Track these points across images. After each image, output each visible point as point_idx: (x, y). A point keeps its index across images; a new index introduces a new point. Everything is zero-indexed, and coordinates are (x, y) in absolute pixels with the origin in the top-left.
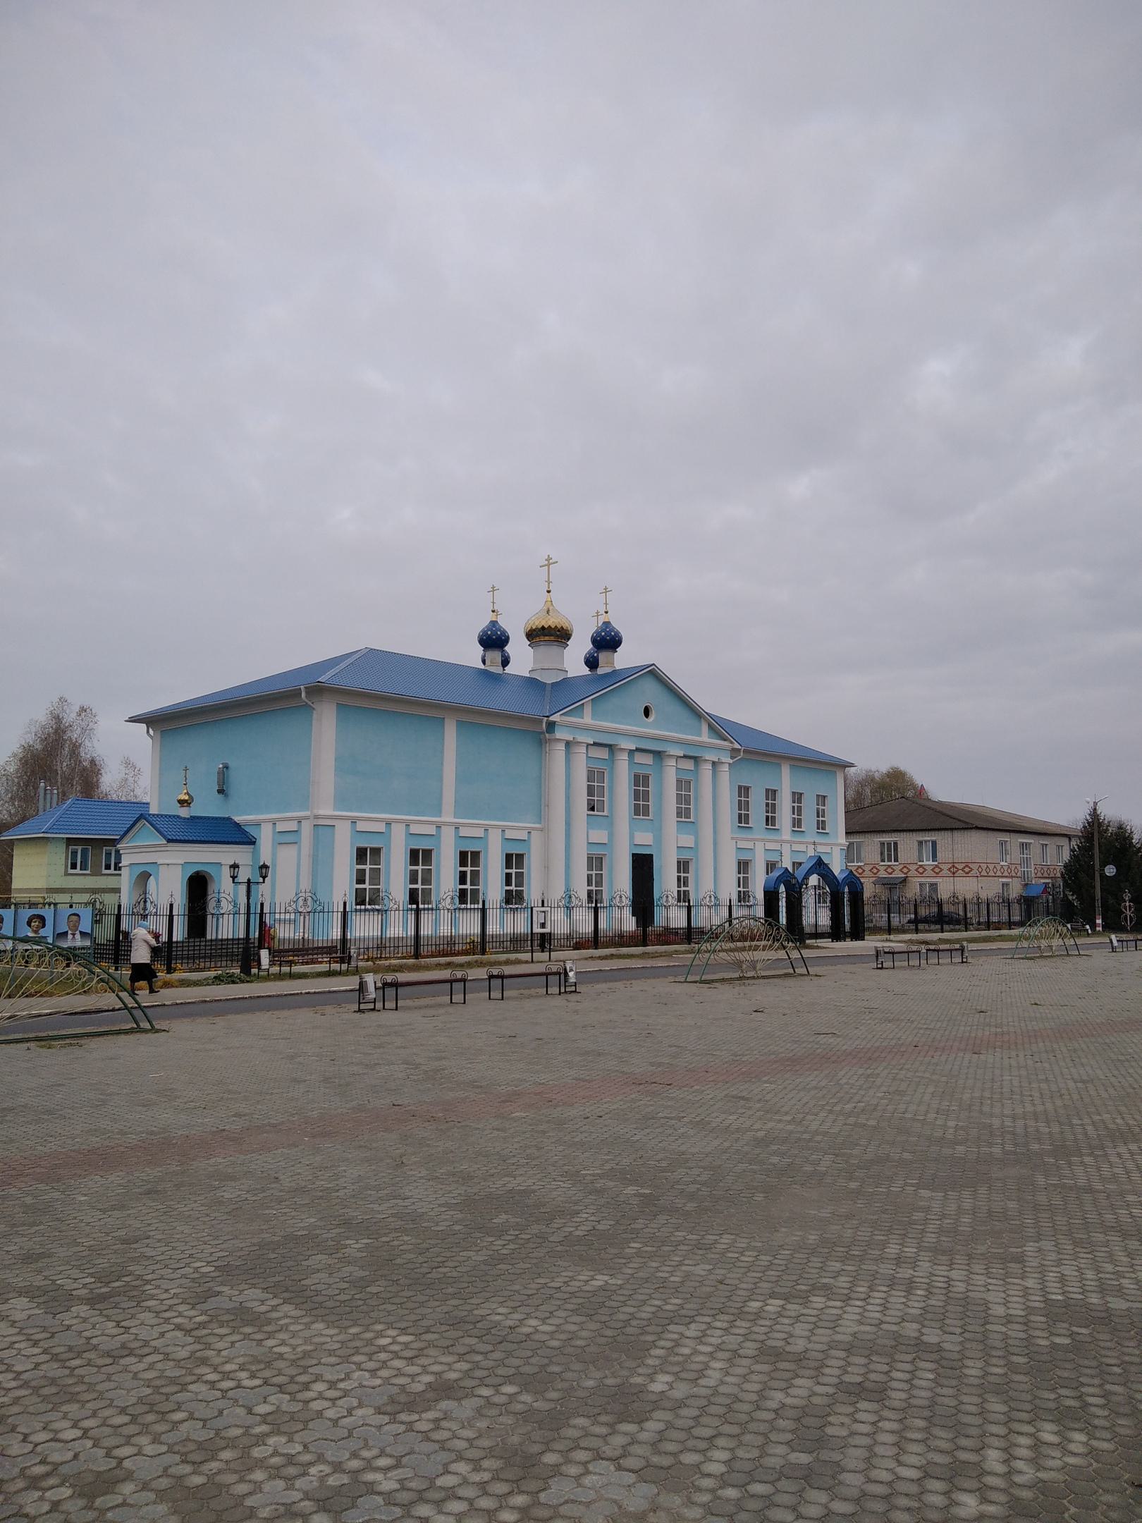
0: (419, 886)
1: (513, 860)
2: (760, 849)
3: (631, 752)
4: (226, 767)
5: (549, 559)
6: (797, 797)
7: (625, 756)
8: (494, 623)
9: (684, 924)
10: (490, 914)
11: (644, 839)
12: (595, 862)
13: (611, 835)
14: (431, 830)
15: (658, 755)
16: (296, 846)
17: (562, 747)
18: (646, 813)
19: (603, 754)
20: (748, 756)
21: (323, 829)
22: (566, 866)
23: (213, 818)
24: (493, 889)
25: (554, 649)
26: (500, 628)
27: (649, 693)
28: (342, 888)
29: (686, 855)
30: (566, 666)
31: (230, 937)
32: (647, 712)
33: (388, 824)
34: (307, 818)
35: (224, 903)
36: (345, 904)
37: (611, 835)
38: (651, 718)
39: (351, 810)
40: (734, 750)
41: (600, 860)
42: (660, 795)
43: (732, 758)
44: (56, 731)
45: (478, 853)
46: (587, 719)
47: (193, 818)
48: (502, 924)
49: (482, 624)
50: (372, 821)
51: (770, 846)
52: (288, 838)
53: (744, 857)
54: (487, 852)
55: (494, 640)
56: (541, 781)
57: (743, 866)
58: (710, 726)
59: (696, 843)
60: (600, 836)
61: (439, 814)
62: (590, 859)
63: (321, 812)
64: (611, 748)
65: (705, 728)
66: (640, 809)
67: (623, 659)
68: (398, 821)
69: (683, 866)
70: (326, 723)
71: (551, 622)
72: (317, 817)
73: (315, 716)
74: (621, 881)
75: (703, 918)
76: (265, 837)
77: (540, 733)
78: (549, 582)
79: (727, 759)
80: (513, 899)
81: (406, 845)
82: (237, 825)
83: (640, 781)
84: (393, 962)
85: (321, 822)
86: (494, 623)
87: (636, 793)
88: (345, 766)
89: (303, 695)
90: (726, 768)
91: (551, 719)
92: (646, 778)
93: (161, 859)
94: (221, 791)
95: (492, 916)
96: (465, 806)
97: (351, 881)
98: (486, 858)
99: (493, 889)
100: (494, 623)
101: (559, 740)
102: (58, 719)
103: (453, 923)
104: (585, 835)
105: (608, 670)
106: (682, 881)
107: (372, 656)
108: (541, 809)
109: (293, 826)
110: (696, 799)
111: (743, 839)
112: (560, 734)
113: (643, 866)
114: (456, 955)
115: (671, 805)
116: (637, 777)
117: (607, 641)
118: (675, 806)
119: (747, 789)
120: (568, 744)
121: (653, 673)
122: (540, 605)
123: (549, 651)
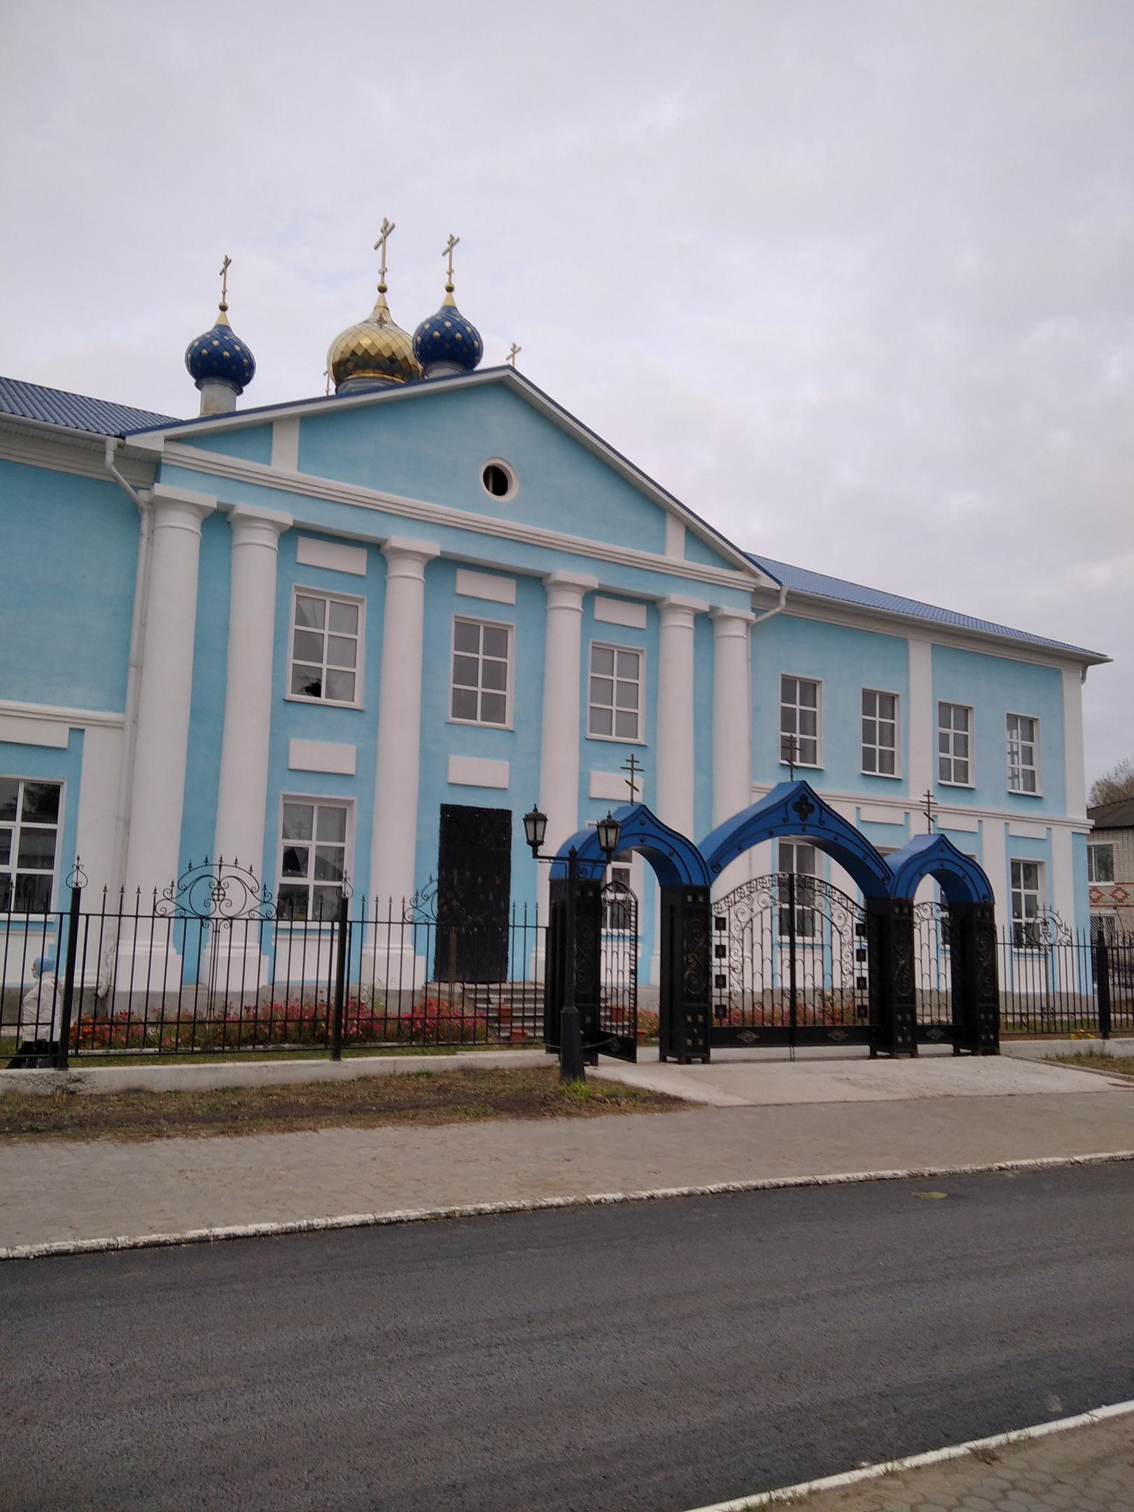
3: (591, 595)
6: (953, 715)
7: (573, 600)
8: (223, 330)
11: (480, 774)
15: (535, 584)
18: (495, 709)
35: (234, 892)
42: (539, 676)
49: (204, 325)
56: (127, 610)
65: (675, 535)
74: (396, 869)
79: (738, 608)
81: (424, 792)
90: (738, 629)
98: (76, 798)
108: (121, 677)
110: (278, 643)
111: (947, 811)
116: (466, 633)
118: (509, 693)
122: (364, 310)
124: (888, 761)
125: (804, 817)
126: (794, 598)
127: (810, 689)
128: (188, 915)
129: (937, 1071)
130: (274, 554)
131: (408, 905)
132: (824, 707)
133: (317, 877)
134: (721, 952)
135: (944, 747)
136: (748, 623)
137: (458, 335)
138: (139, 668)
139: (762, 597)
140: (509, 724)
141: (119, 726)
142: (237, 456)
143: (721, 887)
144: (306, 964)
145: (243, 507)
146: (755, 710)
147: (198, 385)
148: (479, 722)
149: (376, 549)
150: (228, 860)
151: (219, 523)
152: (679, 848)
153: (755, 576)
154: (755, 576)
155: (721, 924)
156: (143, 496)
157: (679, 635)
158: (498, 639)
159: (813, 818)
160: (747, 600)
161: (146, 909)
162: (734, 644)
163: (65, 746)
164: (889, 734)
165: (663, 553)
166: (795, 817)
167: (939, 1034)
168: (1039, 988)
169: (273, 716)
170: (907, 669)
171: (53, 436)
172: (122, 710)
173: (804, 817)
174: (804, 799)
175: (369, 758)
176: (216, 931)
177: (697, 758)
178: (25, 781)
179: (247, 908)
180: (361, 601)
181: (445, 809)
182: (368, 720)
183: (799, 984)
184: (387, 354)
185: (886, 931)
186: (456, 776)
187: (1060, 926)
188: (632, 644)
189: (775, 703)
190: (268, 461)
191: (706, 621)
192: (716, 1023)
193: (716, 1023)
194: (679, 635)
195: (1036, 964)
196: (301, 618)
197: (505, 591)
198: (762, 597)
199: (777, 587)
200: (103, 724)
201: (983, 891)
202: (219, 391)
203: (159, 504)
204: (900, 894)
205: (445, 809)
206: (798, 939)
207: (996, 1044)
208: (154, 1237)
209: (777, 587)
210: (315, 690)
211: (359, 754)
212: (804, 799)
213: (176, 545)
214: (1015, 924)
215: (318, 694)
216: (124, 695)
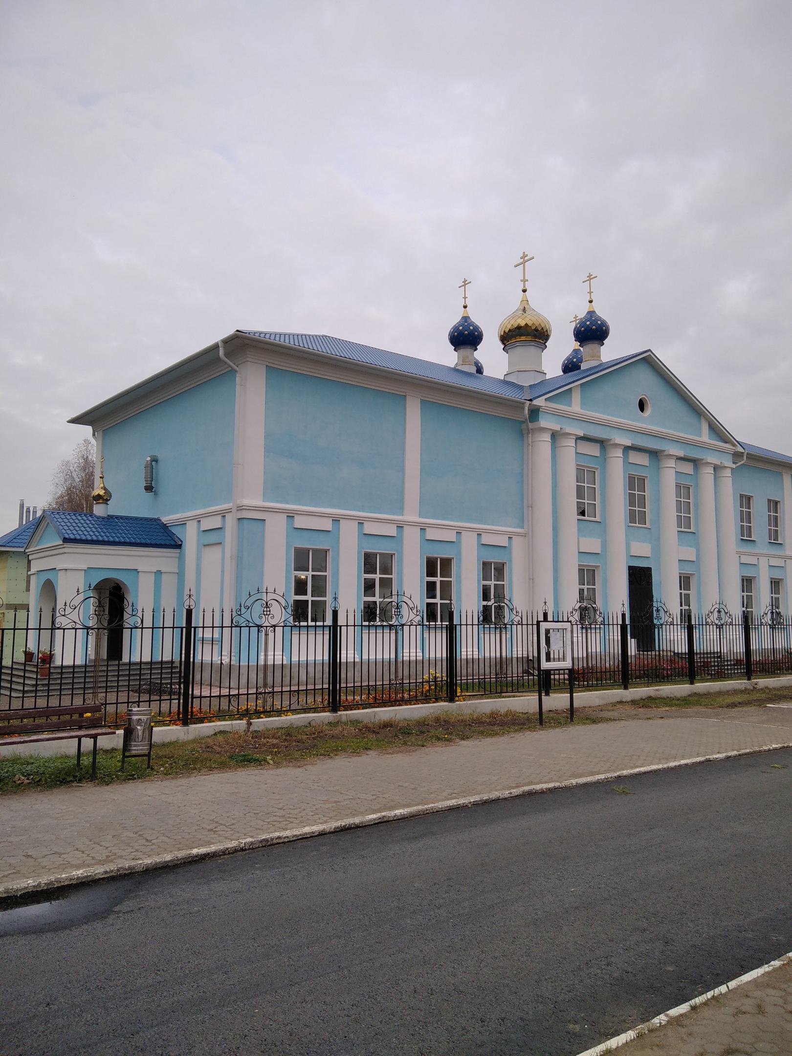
1: (493, 569)
2: (763, 564)
3: (627, 449)
4: (155, 460)
5: (524, 256)
7: (619, 453)
9: (683, 648)
11: (642, 550)
12: (587, 575)
13: (604, 545)
15: (655, 454)
16: (178, 551)
17: (547, 437)
18: (643, 519)
19: (594, 450)
20: (752, 463)
21: (251, 523)
22: (553, 576)
23: (146, 519)
24: (468, 602)
25: (531, 350)
26: (472, 324)
27: (644, 383)
29: (688, 570)
30: (545, 369)
31: (147, 658)
32: (642, 406)
33: (336, 521)
34: (229, 511)
35: (275, 609)
37: (604, 545)
38: (648, 412)
39: (287, 503)
41: (592, 572)
42: (658, 500)
44: (84, 469)
46: (576, 406)
48: (477, 646)
49: (453, 320)
50: (315, 516)
51: (775, 562)
52: (212, 538)
53: (749, 573)
54: (460, 560)
55: (465, 338)
57: (747, 583)
59: (698, 556)
60: (592, 545)
61: (401, 510)
62: (581, 571)
63: (247, 502)
64: (602, 443)
66: (636, 517)
67: (610, 351)
69: (685, 582)
70: (252, 387)
72: (240, 508)
74: (616, 600)
75: (708, 641)
76: (190, 537)
78: (524, 281)
79: (728, 462)
80: (492, 617)
82: (165, 527)
83: (635, 483)
85: (246, 514)
86: (466, 319)
87: (632, 497)
88: (275, 446)
90: (728, 473)
91: (535, 402)
92: (642, 480)
93: (59, 562)
94: (149, 488)
95: (348, 637)
96: (427, 505)
98: (459, 567)
99: (468, 602)
100: (466, 319)
102: (86, 460)
103: (286, 646)
104: (576, 542)
105: (594, 363)
106: (685, 600)
108: (523, 511)
109: (216, 522)
111: (745, 554)
112: (544, 422)
113: (640, 580)
114: (402, 702)
115: (670, 514)
117: (592, 332)
119: (749, 498)
120: (555, 436)
121: (647, 361)
122: (514, 305)
123: (524, 352)
126: (751, 457)
128: (251, 625)
131: (234, 614)
133: (441, 599)
139: (737, 456)
141: (524, 535)
147: (455, 350)
148: (637, 525)
150: (271, 590)
153: (734, 445)
168: (388, 655)
170: (783, 489)
171: (306, 356)
172: (522, 527)
176: (267, 635)
178: (495, 563)
179: (283, 620)
180: (597, 469)
183: (753, 646)
184: (533, 328)
186: (634, 553)
187: (726, 613)
188: (688, 483)
195: (493, 636)
198: (737, 456)
200: (518, 534)
202: (466, 351)
208: (452, 802)
209: (743, 451)
214: (428, 604)
215: (584, 515)
216: (523, 521)
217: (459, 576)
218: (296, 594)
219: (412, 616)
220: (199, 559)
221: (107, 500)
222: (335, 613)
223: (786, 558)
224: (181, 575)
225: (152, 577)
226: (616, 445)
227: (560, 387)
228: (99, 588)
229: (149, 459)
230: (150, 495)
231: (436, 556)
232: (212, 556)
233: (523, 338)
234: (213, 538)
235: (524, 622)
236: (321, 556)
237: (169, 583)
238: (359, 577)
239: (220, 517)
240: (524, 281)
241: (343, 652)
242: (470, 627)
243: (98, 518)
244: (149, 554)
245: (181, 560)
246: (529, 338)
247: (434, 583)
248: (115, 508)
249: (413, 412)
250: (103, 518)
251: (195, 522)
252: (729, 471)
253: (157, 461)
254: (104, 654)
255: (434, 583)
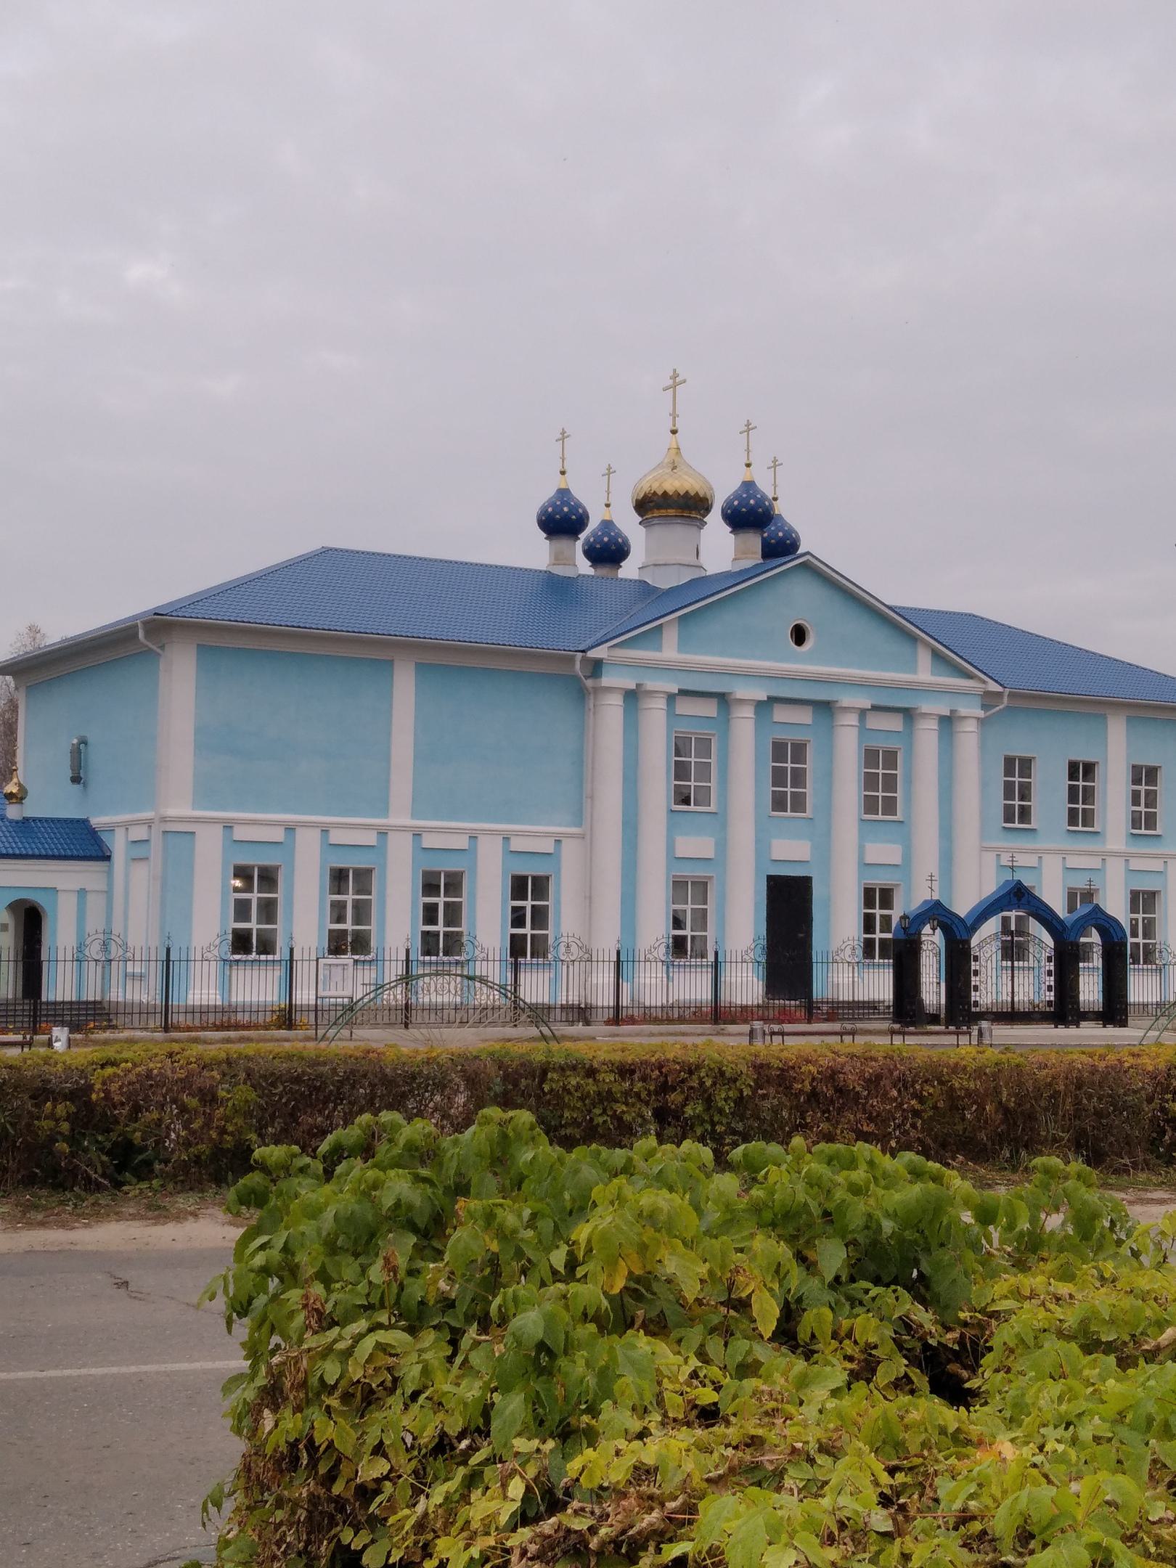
0: (527, 930)
1: (528, 889)
3: (671, 698)
7: (852, 719)
8: (564, 493)
10: (298, 967)
11: (792, 852)
14: (370, 838)
15: (825, 708)
16: (106, 863)
17: (616, 701)
21: (179, 838)
28: (209, 922)
32: (799, 635)
35: (574, 948)
36: (408, 951)
39: (224, 809)
40: (988, 694)
42: (828, 776)
43: (985, 707)
45: (369, 872)
46: (669, 650)
47: (26, 820)
49: (542, 495)
50: (260, 826)
58: (936, 655)
60: (696, 845)
61: (385, 811)
63: (172, 812)
65: (924, 658)
68: (306, 825)
70: (180, 677)
71: (672, 484)
72: (164, 820)
73: (161, 667)
74: (741, 926)
76: (118, 846)
77: (576, 680)
78: (674, 416)
84: (138, 1034)
88: (210, 741)
89: (141, 634)
90: (971, 726)
94: (76, 779)
95: (304, 973)
97: (414, 918)
98: (558, 884)
101: (609, 689)
103: (226, 985)
107: (329, 565)
108: (580, 807)
110: (909, 781)
113: (789, 902)
116: (779, 750)
118: (809, 790)
123: (674, 535)
124: (1088, 818)
125: (1019, 900)
127: (1026, 765)
129: (1091, 1034)
130: (621, 710)
132: (1037, 779)
134: (976, 973)
135: (1136, 801)
136: (978, 719)
137: (752, 502)
138: (592, 798)
140: (809, 814)
141: (583, 837)
142: (646, 649)
143: (974, 941)
144: (693, 987)
145: (650, 685)
146: (984, 785)
149: (723, 699)
151: (633, 697)
152: (956, 921)
153: (984, 682)
154: (984, 682)
155: (976, 959)
156: (589, 683)
157: (927, 734)
158: (799, 751)
159: (1024, 900)
160: (978, 701)
161: (642, 959)
162: (969, 736)
163: (551, 851)
164: (1089, 795)
165: (915, 672)
166: (1014, 900)
167: (1091, 1016)
169: (860, 830)
172: (580, 825)
173: (1019, 900)
174: (1019, 890)
175: (722, 846)
177: (941, 828)
181: (770, 879)
182: (720, 820)
183: (1016, 999)
185: (1067, 961)
186: (776, 855)
189: (999, 778)
190: (915, 672)
191: (948, 722)
192: (973, 1009)
193: (973, 1009)
194: (927, 734)
196: (678, 754)
197: (804, 716)
199: (999, 689)
200: (571, 836)
201: (1120, 935)
203: (598, 690)
204: (1072, 939)
205: (770, 879)
206: (1016, 964)
207: (1126, 1020)
209: (999, 689)
210: (686, 801)
211: (716, 844)
212: (1019, 890)
213: (611, 712)
217: (473, 896)
218: (513, 899)
219: (581, 954)
220: (127, 875)
221: (22, 799)
222: (716, 954)
223: (1165, 858)
224: (109, 893)
225: (73, 899)
226: (742, 701)
227: (712, 595)
228: (14, 907)
229: (75, 741)
230: (76, 786)
231: (251, 863)
232: (141, 874)
233: (663, 512)
234: (139, 851)
235: (594, 959)
236: (541, 886)
237: (95, 904)
238: (504, 902)
239: (145, 827)
240: (674, 416)
241: (299, 992)
242: (394, 958)
243: (11, 821)
244: (69, 868)
245: (110, 874)
246: (671, 512)
247: (249, 901)
248: (31, 809)
249: (404, 683)
250: (17, 822)
251: (123, 829)
252: (974, 722)
253: (85, 743)
254: (20, 994)
255: (249, 901)
